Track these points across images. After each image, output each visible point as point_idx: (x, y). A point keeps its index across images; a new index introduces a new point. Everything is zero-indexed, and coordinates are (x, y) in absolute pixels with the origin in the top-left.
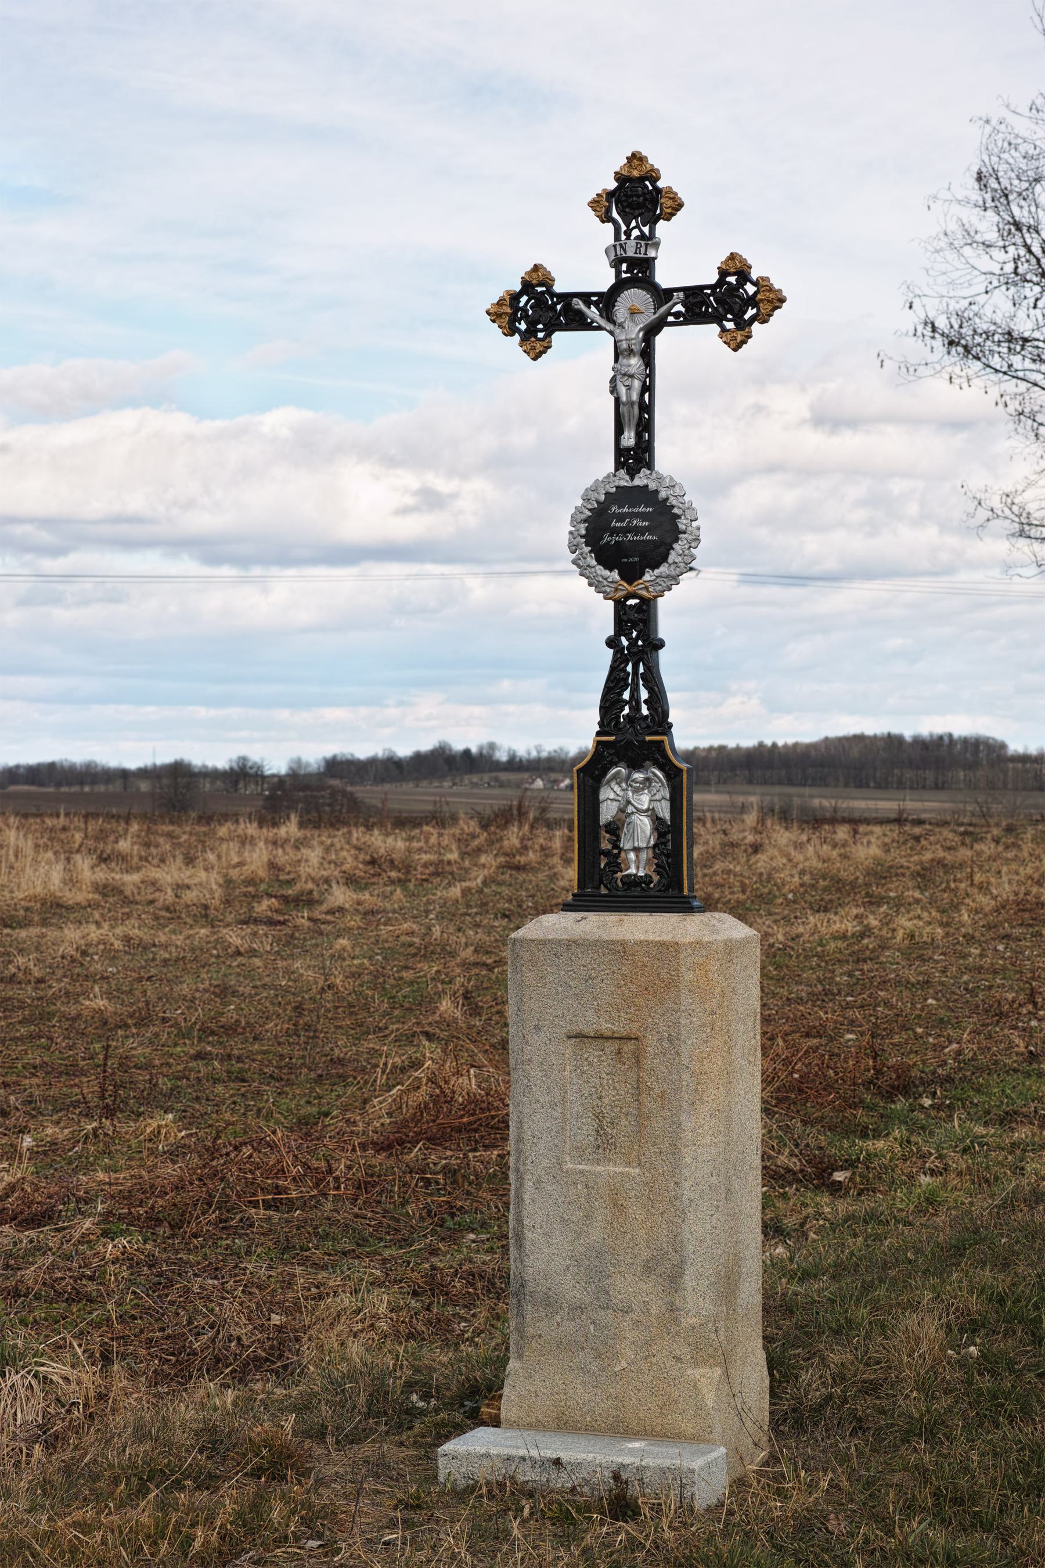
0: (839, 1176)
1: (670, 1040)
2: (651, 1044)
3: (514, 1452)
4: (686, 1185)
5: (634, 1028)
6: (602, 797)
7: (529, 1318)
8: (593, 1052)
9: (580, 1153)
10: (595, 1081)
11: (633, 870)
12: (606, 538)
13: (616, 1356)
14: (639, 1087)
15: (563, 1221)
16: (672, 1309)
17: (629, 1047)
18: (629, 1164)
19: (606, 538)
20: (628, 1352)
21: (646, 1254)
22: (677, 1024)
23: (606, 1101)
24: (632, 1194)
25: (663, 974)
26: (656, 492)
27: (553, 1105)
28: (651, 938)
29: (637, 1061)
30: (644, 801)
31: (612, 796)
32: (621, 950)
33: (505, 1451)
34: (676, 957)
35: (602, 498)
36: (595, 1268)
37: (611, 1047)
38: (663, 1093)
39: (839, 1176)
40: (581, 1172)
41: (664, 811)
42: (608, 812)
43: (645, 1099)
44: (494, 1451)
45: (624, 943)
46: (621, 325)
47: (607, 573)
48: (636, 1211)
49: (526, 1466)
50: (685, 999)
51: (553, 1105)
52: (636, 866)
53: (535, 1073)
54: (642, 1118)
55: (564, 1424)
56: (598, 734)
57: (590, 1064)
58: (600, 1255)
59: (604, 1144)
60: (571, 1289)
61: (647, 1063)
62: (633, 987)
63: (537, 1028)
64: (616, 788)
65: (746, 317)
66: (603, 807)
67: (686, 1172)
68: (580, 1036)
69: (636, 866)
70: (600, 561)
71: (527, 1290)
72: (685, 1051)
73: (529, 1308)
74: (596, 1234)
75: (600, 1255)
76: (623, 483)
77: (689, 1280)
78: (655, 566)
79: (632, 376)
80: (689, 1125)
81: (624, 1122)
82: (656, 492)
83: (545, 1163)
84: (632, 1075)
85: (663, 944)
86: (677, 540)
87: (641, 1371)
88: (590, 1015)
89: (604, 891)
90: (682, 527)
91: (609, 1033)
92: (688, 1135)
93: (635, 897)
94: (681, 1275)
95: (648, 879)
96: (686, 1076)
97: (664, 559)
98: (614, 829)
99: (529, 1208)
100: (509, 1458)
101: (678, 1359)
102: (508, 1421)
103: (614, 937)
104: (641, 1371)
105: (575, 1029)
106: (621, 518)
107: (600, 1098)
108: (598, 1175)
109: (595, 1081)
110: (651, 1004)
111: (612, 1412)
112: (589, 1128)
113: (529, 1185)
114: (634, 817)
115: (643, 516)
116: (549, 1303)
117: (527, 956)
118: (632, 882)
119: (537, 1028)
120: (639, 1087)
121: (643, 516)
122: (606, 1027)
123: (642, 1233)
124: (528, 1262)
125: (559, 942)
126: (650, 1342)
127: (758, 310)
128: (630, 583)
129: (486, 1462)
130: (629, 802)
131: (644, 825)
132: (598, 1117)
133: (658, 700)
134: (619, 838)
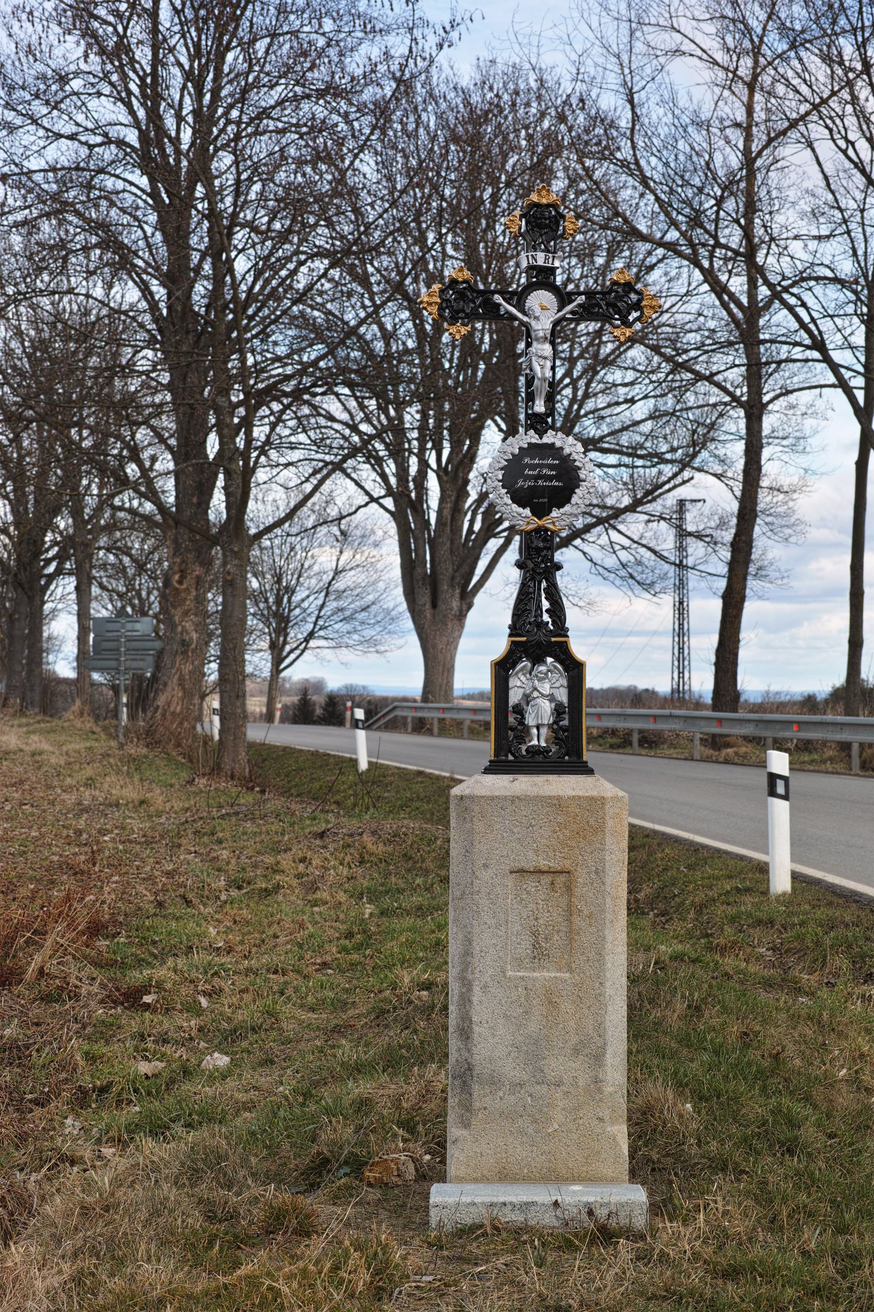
0: (147, 999)
1: (597, 873)
2: (582, 877)
3: (495, 1200)
4: (608, 984)
5: (567, 864)
6: (511, 684)
7: (475, 1095)
8: (531, 884)
9: (519, 963)
10: (532, 906)
11: (535, 742)
12: (520, 483)
13: (549, 1120)
14: (570, 911)
15: (505, 1016)
16: (597, 1081)
17: (561, 879)
18: (559, 970)
19: (520, 483)
20: (560, 1117)
21: (574, 1040)
22: (603, 860)
23: (541, 921)
24: (564, 993)
25: (592, 822)
26: (562, 448)
27: (498, 926)
28: (581, 794)
29: (569, 889)
30: (546, 688)
31: (519, 684)
32: (558, 803)
33: (488, 1200)
34: (603, 808)
35: (517, 451)
36: (533, 1053)
37: (546, 879)
38: (591, 913)
39: (147, 999)
40: (522, 978)
41: (563, 696)
42: (515, 697)
43: (576, 919)
44: (478, 1200)
45: (559, 798)
46: (537, 318)
47: (520, 510)
48: (566, 1007)
49: (507, 1210)
50: (609, 840)
51: (498, 926)
52: (539, 739)
53: (484, 902)
54: (571, 934)
55: (505, 1176)
56: (510, 635)
57: (528, 893)
58: (536, 1043)
59: (539, 954)
60: (512, 1070)
61: (578, 891)
62: (567, 832)
63: (485, 866)
64: (523, 678)
65: (631, 318)
66: (511, 693)
67: (608, 975)
68: (522, 871)
69: (539, 739)
70: (514, 501)
71: (475, 1073)
72: (608, 880)
73: (476, 1089)
74: (533, 1027)
75: (536, 1043)
76: (534, 441)
77: (609, 1059)
78: (560, 506)
79: (545, 358)
80: (609, 938)
81: (556, 937)
82: (562, 448)
83: (491, 971)
84: (563, 902)
85: (592, 798)
86: (578, 487)
87: (571, 1131)
88: (531, 854)
89: (511, 758)
90: (582, 476)
91: (546, 869)
92: (609, 946)
93: (537, 763)
94: (604, 1054)
95: (546, 750)
96: (608, 900)
97: (568, 501)
98: (519, 710)
99: (477, 1008)
100: (492, 1205)
101: (601, 1120)
102: (457, 1177)
103: (548, 793)
104: (571, 1131)
105: (518, 865)
106: (533, 467)
107: (536, 919)
108: (535, 980)
109: (532, 906)
110: (582, 845)
111: (547, 1165)
112: (526, 943)
113: (476, 990)
114: (538, 701)
115: (551, 467)
116: (494, 1082)
117: (477, 809)
118: (535, 751)
119: (485, 866)
120: (570, 911)
121: (551, 467)
122: (543, 863)
123: (572, 1023)
124: (475, 1050)
125: (505, 798)
126: (577, 1109)
127: (642, 313)
128: (540, 518)
129: (472, 1209)
130: (535, 689)
131: (546, 708)
132: (535, 934)
133: (558, 611)
134: (523, 717)
